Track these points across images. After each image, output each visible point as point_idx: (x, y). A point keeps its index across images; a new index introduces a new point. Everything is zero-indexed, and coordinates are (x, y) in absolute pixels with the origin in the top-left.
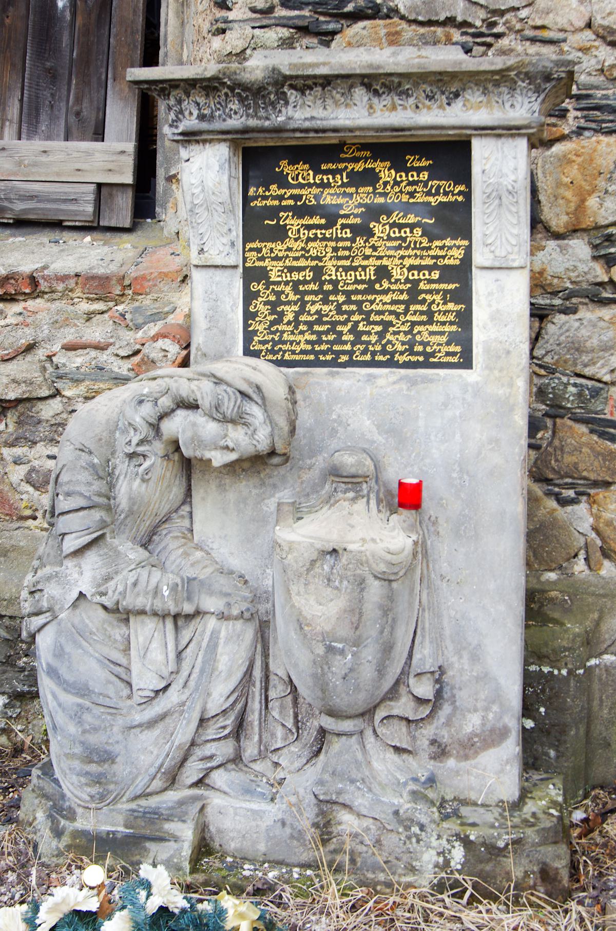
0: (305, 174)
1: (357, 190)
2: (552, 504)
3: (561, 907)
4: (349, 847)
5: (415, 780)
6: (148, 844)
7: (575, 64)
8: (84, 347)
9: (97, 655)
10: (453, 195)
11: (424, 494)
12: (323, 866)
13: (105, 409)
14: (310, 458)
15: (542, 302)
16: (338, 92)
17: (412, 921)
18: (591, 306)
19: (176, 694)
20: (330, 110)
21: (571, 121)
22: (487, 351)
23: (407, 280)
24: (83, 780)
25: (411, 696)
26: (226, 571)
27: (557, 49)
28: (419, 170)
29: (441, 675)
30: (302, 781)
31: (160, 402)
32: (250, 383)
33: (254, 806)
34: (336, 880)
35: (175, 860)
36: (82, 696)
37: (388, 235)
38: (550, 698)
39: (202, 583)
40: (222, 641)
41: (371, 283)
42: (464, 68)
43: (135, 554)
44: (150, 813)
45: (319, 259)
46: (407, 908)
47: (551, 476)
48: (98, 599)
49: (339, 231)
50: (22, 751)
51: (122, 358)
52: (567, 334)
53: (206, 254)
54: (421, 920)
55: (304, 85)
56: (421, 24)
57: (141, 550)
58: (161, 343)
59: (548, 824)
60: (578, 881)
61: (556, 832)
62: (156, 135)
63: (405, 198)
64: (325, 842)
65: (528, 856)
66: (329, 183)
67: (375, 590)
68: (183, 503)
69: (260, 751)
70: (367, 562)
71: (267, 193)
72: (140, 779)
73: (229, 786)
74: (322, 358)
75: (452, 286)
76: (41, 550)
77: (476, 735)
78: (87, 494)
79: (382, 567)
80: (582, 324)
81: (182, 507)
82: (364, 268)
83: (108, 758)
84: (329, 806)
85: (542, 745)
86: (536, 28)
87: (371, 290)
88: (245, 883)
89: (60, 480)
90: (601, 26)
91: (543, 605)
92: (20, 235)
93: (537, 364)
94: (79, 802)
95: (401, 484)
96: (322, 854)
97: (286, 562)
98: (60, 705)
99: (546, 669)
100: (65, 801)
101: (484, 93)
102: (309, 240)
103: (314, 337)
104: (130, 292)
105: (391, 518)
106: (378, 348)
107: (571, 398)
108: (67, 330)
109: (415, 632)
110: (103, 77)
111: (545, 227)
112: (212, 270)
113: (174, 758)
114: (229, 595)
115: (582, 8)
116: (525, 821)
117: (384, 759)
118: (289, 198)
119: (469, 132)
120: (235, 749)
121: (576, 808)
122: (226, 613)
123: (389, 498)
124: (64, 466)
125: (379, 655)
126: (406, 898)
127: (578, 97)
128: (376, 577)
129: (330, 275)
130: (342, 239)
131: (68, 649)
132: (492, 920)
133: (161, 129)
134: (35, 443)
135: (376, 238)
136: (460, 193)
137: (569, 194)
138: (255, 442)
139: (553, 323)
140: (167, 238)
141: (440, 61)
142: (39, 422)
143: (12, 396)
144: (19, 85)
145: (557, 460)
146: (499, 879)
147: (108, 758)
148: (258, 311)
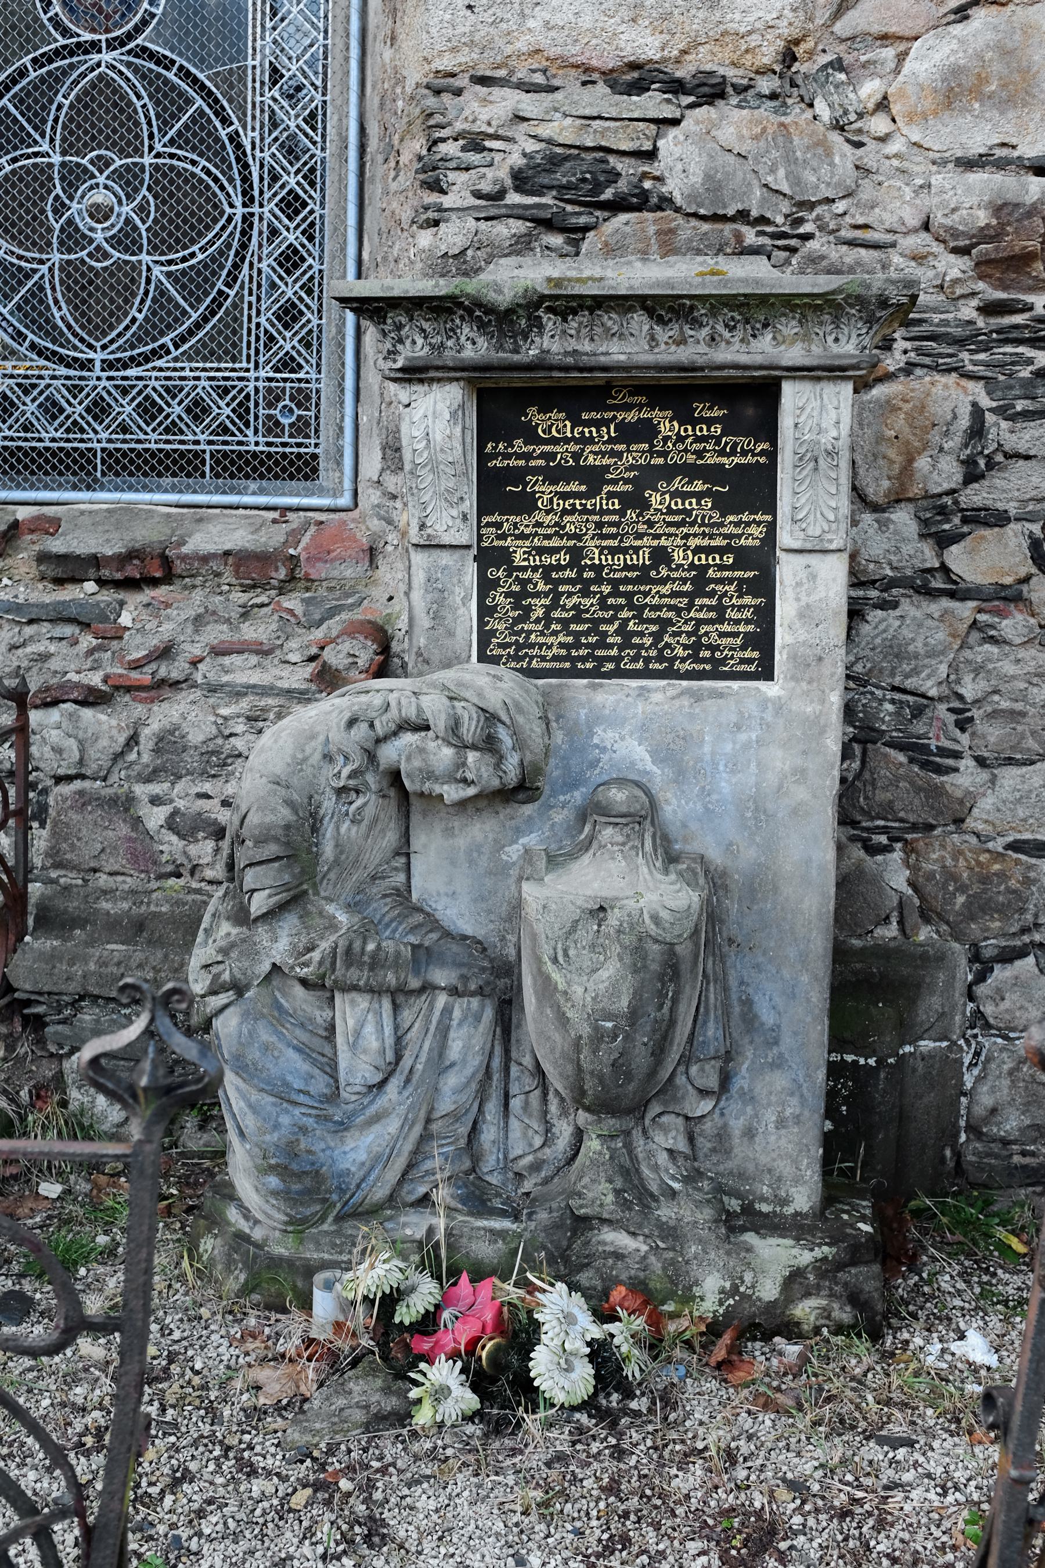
18: (916, 598)
22: (793, 657)
23: (692, 566)
28: (710, 422)
37: (669, 507)
52: (529, 104)
56: (704, 218)
66: (592, 437)
74: (579, 665)
82: (636, 550)
87: (644, 578)
90: (942, 226)
98: (250, 1106)
99: (849, 1058)
102: (565, 512)
106: (653, 653)
112: (438, 551)
118: (539, 457)
130: (609, 512)
136: (762, 453)
137: (892, 453)
145: (866, 798)
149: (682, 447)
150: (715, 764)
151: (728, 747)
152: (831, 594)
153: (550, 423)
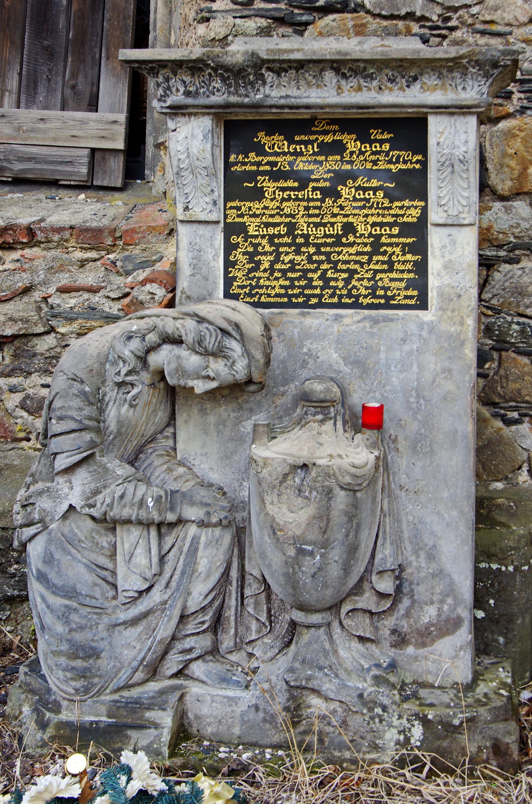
0: (280, 144)
1: (326, 158)
2: (499, 424)
3: (512, 779)
4: (317, 728)
5: (378, 666)
6: (129, 732)
7: (519, 53)
8: (77, 290)
9: (85, 560)
10: (411, 163)
11: (385, 416)
12: (293, 746)
13: (96, 344)
14: (283, 386)
15: (489, 254)
16: (310, 75)
17: (376, 795)
19: (158, 594)
20: (303, 90)
21: (515, 102)
22: (441, 294)
23: (370, 235)
24: (69, 675)
25: (373, 591)
26: (206, 484)
27: (504, 40)
28: (382, 142)
29: (400, 572)
30: (274, 669)
31: (147, 338)
32: (229, 322)
33: (230, 693)
34: (305, 759)
35: (155, 746)
36: (70, 598)
37: (354, 197)
38: (498, 591)
39: (184, 495)
40: (201, 546)
41: (338, 237)
42: (422, 56)
43: (123, 470)
44: (131, 703)
45: (293, 216)
46: (371, 783)
47: (497, 400)
48: (87, 510)
49: (310, 193)
50: (11, 650)
51: (113, 299)
53: (191, 211)
54: (383, 794)
55: (280, 68)
56: (385, 18)
57: (127, 466)
58: (148, 287)
59: (499, 704)
60: (527, 754)
61: (506, 711)
62: (146, 108)
63: (369, 166)
64: (295, 724)
65: (481, 732)
67: (341, 498)
68: (168, 425)
69: (236, 643)
70: (334, 475)
71: (246, 160)
72: (123, 672)
73: (206, 676)
75: (410, 240)
76: (34, 468)
77: (433, 625)
78: (79, 418)
79: (348, 479)
80: (524, 272)
81: (167, 429)
82: (332, 224)
83: (94, 653)
84: (299, 691)
85: (492, 632)
86: (485, 22)
87: (338, 243)
88: (220, 765)
89: (53, 406)
91: (491, 511)
92: (18, 192)
93: (484, 306)
94: (64, 695)
95: (364, 407)
96: (292, 735)
97: (261, 475)
98: (48, 607)
99: (494, 566)
100: (50, 695)
101: (439, 78)
102: (283, 200)
103: (287, 283)
104: (121, 243)
105: (355, 437)
106: (344, 292)
107: (515, 334)
108: (61, 275)
109: (377, 535)
110: (97, 56)
111: (492, 191)
113: (155, 652)
114: (209, 505)
115: (526, 6)
116: (478, 701)
117: (349, 647)
119: (425, 110)
120: (213, 642)
121: (524, 689)
122: (206, 521)
123: (354, 420)
124: (57, 393)
125: (345, 556)
126: (370, 774)
127: (522, 82)
128: (342, 488)
129: (302, 230)
130: (313, 200)
131: (57, 556)
132: (449, 792)
133: (151, 103)
134: (30, 374)
135: (343, 199)
136: (417, 162)
138: (233, 372)
139: (499, 271)
140: (155, 197)
141: (401, 50)
142: (35, 355)
143: (8, 332)
144: (18, 60)
145: (502, 387)
146: (455, 754)
147: (94, 653)
148: (237, 260)
149: (362, 158)
150: (388, 366)
151: (398, 355)
152: (466, 253)
153: (276, 143)
